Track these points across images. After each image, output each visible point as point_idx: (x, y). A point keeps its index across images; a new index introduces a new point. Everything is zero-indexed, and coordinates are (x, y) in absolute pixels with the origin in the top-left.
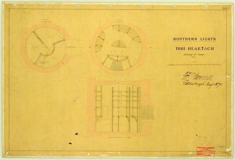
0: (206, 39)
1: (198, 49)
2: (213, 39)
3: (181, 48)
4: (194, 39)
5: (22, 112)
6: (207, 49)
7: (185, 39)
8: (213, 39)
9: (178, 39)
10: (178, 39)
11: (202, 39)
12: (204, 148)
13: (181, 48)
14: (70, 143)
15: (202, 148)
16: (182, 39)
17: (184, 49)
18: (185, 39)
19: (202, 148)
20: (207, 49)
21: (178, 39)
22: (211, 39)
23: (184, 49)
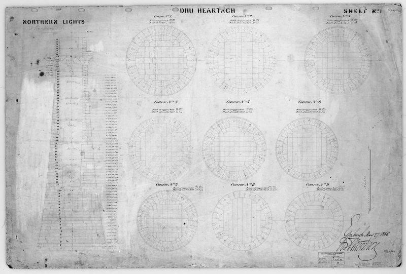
0: (71, 22)
1: (211, 11)
2: (81, 22)
3: (187, 10)
4: (53, 22)
5: (210, 86)
6: (225, 11)
7: (40, 22)
8: (81, 22)
9: (29, 22)
10: (29, 22)
11: (65, 22)
12: (329, 253)
13: (187, 10)
14: (46, 265)
15: (326, 253)
16: (36, 22)
17: (191, 11)
18: (40, 22)
19: (326, 253)
20: (225, 11)
21: (29, 22)
22: (78, 22)
23: (191, 11)
